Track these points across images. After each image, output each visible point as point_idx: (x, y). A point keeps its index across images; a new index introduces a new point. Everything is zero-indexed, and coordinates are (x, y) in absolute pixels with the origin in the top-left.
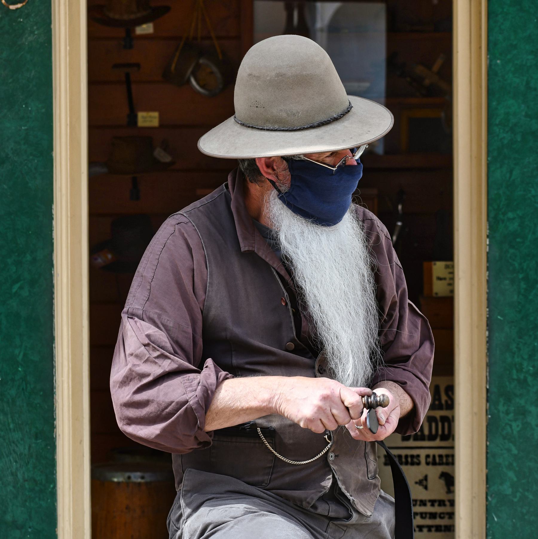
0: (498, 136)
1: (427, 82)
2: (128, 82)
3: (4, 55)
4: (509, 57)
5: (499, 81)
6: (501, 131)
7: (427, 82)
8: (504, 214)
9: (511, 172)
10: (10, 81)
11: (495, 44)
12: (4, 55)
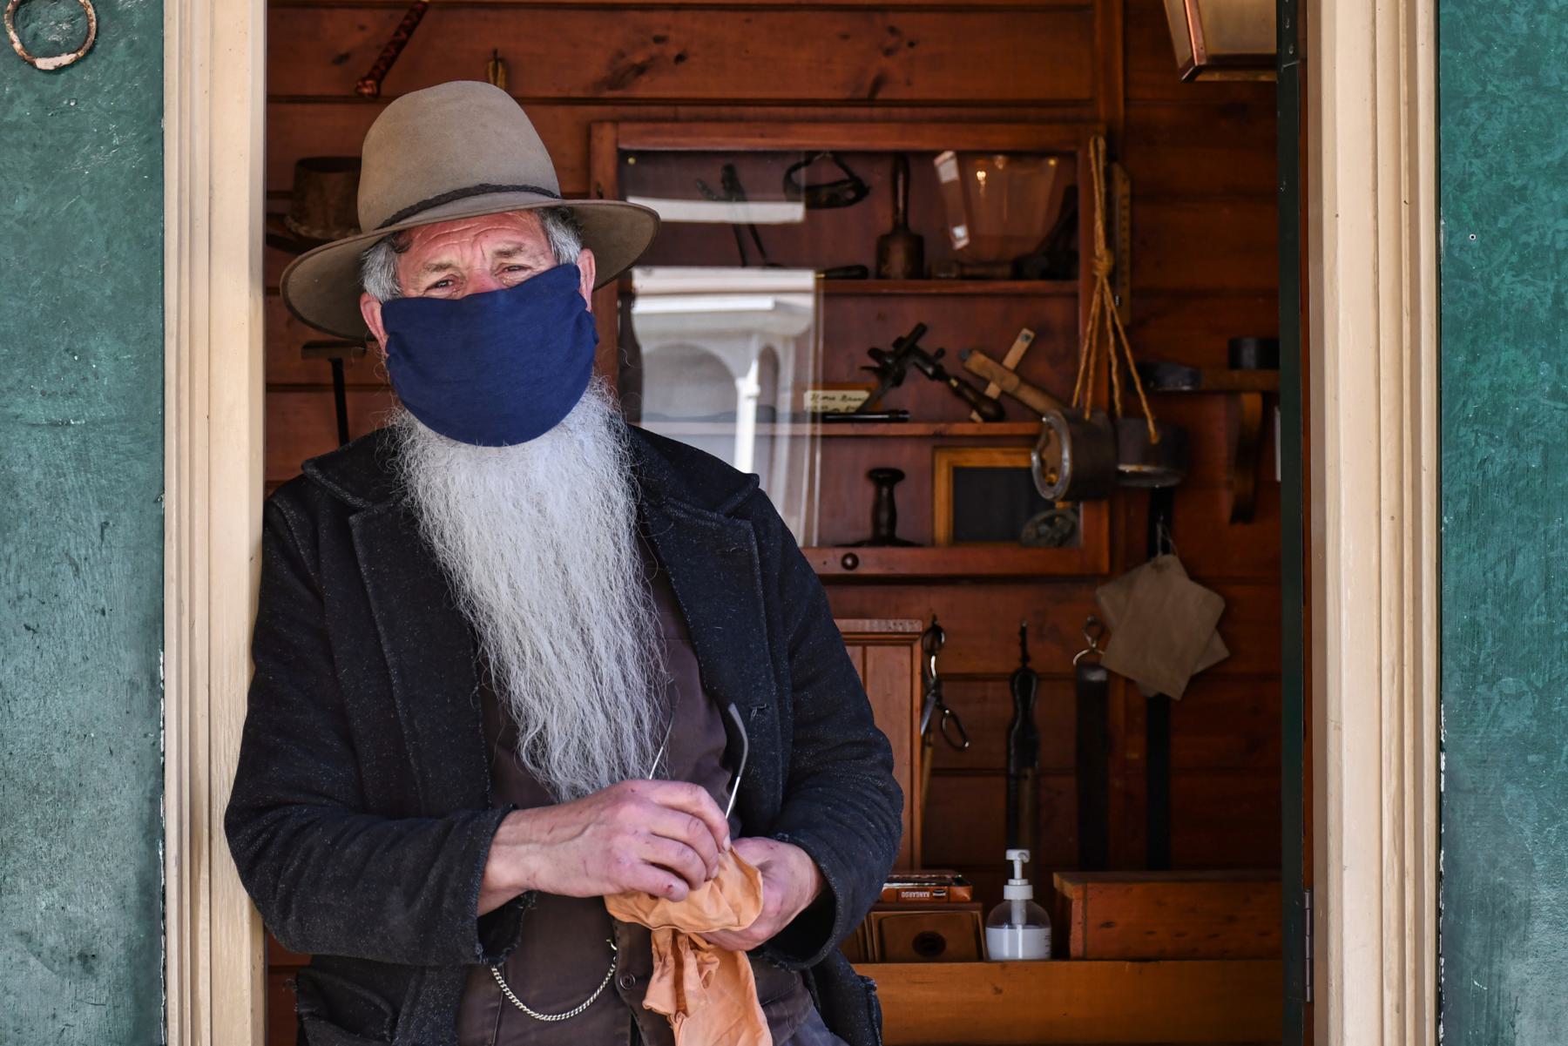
0: (1472, 453)
1: (993, 391)
2: (339, 388)
3: (20, 205)
4: (1502, 223)
5: (1474, 294)
6: (1483, 439)
7: (993, 391)
8: (1492, 680)
9: (1512, 559)
10: (36, 282)
11: (1463, 187)
12: (20, 205)
